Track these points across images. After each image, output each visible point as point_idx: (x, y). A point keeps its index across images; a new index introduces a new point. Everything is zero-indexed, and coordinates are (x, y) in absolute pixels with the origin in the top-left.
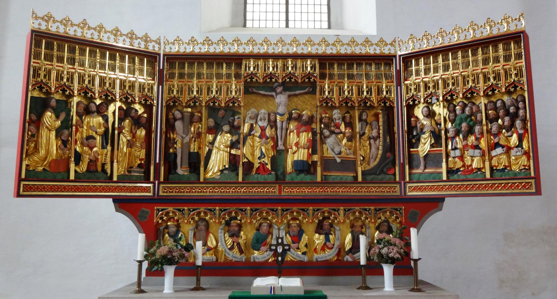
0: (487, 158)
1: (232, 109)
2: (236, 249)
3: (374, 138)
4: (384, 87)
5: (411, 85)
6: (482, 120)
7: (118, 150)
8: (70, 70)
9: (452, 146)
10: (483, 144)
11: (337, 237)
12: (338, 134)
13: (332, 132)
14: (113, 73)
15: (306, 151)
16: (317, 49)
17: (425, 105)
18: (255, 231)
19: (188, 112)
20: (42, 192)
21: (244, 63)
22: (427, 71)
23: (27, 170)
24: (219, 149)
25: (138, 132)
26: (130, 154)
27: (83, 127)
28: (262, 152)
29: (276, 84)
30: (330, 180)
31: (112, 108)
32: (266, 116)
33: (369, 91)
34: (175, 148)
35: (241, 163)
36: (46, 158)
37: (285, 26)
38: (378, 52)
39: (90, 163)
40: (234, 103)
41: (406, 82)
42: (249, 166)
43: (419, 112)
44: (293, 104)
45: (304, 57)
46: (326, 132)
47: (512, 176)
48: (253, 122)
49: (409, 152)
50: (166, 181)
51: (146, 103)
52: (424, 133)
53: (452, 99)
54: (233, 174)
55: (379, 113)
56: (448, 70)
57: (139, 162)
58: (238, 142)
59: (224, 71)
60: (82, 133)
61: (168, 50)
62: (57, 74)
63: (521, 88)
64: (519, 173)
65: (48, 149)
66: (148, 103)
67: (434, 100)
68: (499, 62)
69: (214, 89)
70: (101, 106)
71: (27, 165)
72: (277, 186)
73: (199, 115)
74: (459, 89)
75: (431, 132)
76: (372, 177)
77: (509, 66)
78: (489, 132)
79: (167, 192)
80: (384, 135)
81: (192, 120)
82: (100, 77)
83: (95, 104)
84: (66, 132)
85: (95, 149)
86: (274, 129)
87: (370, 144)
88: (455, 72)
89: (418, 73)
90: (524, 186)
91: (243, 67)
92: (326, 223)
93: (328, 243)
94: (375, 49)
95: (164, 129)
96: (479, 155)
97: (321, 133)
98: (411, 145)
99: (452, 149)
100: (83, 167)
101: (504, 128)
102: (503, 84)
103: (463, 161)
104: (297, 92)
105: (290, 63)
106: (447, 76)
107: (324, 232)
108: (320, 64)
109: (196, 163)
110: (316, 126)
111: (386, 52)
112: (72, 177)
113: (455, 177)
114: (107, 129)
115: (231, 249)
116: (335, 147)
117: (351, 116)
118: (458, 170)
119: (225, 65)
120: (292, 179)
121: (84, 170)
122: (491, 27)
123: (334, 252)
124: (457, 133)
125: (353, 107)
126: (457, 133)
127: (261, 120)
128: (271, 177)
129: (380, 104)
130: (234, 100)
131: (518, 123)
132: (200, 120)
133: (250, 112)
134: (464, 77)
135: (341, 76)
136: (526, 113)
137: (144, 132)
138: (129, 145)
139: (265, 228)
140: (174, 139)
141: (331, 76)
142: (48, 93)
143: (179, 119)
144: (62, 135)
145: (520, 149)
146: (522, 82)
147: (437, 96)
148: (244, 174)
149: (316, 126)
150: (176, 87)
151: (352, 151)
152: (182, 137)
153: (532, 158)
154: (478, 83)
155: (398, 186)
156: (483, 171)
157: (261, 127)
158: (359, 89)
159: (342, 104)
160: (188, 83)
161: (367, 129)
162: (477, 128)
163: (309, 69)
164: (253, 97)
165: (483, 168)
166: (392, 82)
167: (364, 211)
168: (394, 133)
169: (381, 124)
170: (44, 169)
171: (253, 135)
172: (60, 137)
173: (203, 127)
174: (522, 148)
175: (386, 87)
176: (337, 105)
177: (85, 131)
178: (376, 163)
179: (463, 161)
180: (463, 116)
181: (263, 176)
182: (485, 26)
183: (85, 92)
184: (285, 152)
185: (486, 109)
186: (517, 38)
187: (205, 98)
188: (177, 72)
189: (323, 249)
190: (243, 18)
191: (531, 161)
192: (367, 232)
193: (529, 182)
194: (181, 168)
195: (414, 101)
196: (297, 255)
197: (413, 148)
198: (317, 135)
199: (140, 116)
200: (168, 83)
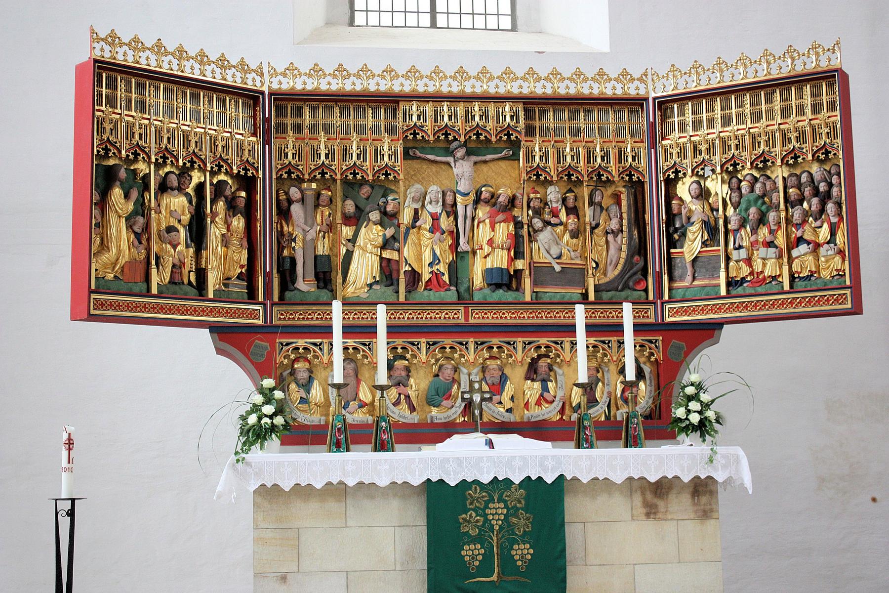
0: (785, 260)
1: (383, 184)
2: (404, 406)
4: (629, 150)
5: (671, 146)
11: (559, 385)
12: (557, 225)
13: (547, 223)
15: (505, 252)
16: (521, 87)
17: (695, 178)
18: (431, 379)
22: (697, 125)
24: (364, 250)
28: (434, 254)
29: (456, 144)
30: (546, 300)
32: (440, 195)
33: (605, 156)
39: (174, 270)
40: (387, 175)
41: (663, 142)
42: (414, 277)
43: (684, 189)
46: (538, 223)
47: (820, 286)
49: (669, 253)
53: (736, 171)
54: (389, 290)
56: (729, 125)
58: (393, 237)
59: (370, 121)
61: (275, 86)
64: (831, 281)
67: (708, 172)
69: (355, 151)
71: (96, 270)
72: (462, 308)
73: (330, 193)
74: (745, 154)
75: (704, 222)
76: (610, 294)
78: (788, 221)
80: (629, 228)
82: (183, 131)
84: (141, 220)
85: (179, 248)
87: (607, 242)
88: (740, 127)
89: (682, 127)
90: (837, 300)
91: (400, 115)
92: (543, 363)
94: (614, 88)
97: (530, 225)
98: (672, 244)
99: (735, 249)
101: (811, 215)
103: (751, 266)
104: (489, 157)
105: (477, 108)
106: (728, 134)
108: (526, 110)
111: (633, 92)
112: (154, 290)
113: (740, 290)
115: (396, 403)
116: (550, 246)
117: (576, 197)
120: (485, 297)
121: (167, 280)
122: (793, 59)
123: (557, 405)
124: (743, 224)
125: (579, 182)
126: (743, 224)
127: (431, 203)
128: (451, 295)
130: (386, 171)
131: (830, 207)
133: (413, 189)
134: (753, 137)
135: (559, 131)
136: (841, 192)
139: (448, 372)
140: (290, 234)
143: (297, 201)
144: (134, 224)
147: (712, 165)
148: (408, 291)
149: (523, 214)
151: (578, 254)
152: (304, 230)
153: (847, 258)
155: (652, 308)
156: (780, 279)
157: (432, 215)
158: (588, 153)
160: (311, 141)
161: (602, 219)
162: (772, 216)
163: (508, 119)
164: (415, 164)
165: (779, 276)
166: (642, 142)
167: (602, 345)
169: (624, 209)
170: (115, 277)
171: (420, 228)
172: (131, 227)
174: (835, 245)
175: (633, 149)
176: (555, 178)
178: (617, 272)
179: (751, 266)
181: (437, 294)
182: (784, 57)
184: (471, 255)
186: (833, 78)
188: (289, 121)
189: (538, 403)
191: (847, 262)
192: (606, 377)
193: (845, 296)
195: (677, 172)
197: (675, 248)
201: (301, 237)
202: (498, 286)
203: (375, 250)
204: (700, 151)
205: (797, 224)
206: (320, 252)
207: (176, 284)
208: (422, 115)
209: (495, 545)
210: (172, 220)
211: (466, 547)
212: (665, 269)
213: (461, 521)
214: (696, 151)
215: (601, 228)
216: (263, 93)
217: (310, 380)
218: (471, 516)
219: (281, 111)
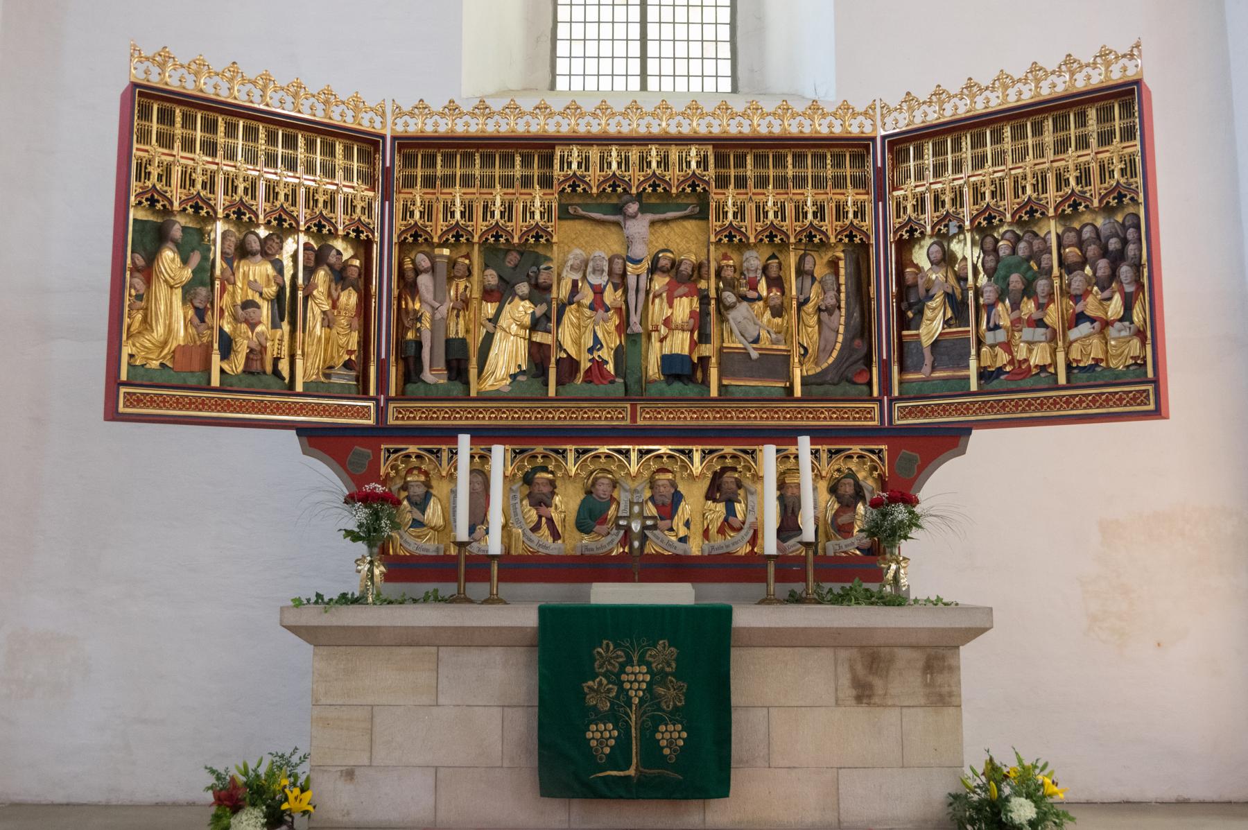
2: (545, 530)
3: (827, 309)
5: (905, 198)
6: (1051, 267)
7: (304, 331)
8: (208, 166)
9: (988, 322)
10: (1053, 316)
12: (753, 300)
13: (744, 298)
14: (291, 174)
19: (442, 256)
20: (161, 408)
21: (558, 153)
22: (939, 170)
25: (343, 298)
26: (327, 340)
27: (234, 284)
30: (737, 396)
31: (290, 246)
34: (418, 330)
35: (553, 360)
36: (165, 343)
37: (638, 88)
42: (569, 367)
43: (921, 256)
44: (661, 240)
45: (683, 141)
48: (577, 276)
49: (900, 337)
50: (402, 396)
51: (358, 236)
52: (931, 298)
54: (537, 383)
55: (839, 259)
57: (347, 357)
58: (547, 316)
60: (233, 294)
61: (400, 129)
62: (184, 173)
63: (1132, 199)
64: (1124, 373)
65: (170, 324)
66: (363, 236)
68: (1087, 146)
70: (270, 243)
71: (131, 356)
73: (467, 261)
75: (947, 294)
77: (1107, 155)
79: (403, 418)
81: (453, 271)
82: (268, 181)
83: (257, 235)
84: (203, 291)
85: (259, 329)
86: (620, 292)
89: (920, 175)
91: (557, 162)
93: (731, 519)
95: (395, 292)
96: (1043, 338)
97: (719, 300)
99: (989, 329)
100: (238, 363)
102: (1095, 189)
103: (1011, 353)
105: (654, 153)
106: (980, 178)
107: (724, 497)
110: (710, 285)
111: (855, 131)
112: (215, 381)
113: (995, 384)
114: (281, 289)
115: (536, 528)
116: (750, 325)
117: (780, 264)
118: (1000, 371)
119: (518, 159)
121: (240, 369)
123: (746, 534)
125: (784, 245)
128: (618, 389)
129: (841, 240)
130: (539, 234)
131: (1125, 271)
132: (469, 273)
136: (1141, 250)
137: (354, 299)
138: (326, 323)
141: (741, 182)
142: (167, 212)
143: (426, 271)
145: (1127, 323)
146: (1133, 187)
148: (559, 383)
149: (710, 285)
150: (418, 203)
153: (1149, 341)
154: (1045, 191)
155: (876, 406)
159: (761, 240)
162: (1041, 284)
164: (578, 225)
165: (1050, 365)
168: (870, 300)
169: (842, 280)
170: (162, 365)
171: (579, 304)
172: (191, 301)
173: (475, 287)
174: (1132, 322)
177: (241, 292)
179: (1011, 353)
180: (1014, 259)
183: (240, 215)
185: (1060, 246)
186: (1126, 96)
187: (479, 225)
188: (419, 172)
189: (721, 531)
190: (548, 68)
191: (1149, 348)
194: (431, 370)
195: (911, 231)
196: (670, 544)
198: (709, 304)
199: (346, 266)
200: (402, 196)
201: (428, 315)
202: (678, 377)
203: (522, 332)
204: (943, 203)
205: (1076, 296)
206: (452, 335)
207: (252, 373)
208: (585, 163)
209: (633, 725)
210: (250, 292)
211: (593, 727)
212: (895, 357)
213: (586, 690)
214: (938, 202)
215: (811, 304)
216: (383, 137)
217: (427, 496)
218: (600, 683)
219: (409, 161)
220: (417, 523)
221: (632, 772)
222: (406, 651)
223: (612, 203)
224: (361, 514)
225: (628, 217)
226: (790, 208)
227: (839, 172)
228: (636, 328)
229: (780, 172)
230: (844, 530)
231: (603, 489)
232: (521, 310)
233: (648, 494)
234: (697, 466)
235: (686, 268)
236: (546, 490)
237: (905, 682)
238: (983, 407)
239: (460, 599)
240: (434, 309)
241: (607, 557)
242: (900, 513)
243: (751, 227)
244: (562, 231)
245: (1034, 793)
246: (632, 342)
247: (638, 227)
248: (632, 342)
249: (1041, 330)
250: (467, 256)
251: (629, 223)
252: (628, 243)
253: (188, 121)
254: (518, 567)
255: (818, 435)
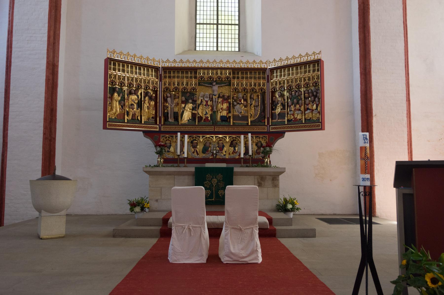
2: (195, 153)
13: (238, 103)
21: (198, 71)
23: (109, 118)
25: (151, 103)
36: (115, 113)
38: (259, 67)
42: (200, 118)
48: (202, 98)
49: (272, 112)
50: (164, 124)
52: (278, 104)
59: (189, 75)
60: (129, 103)
61: (163, 65)
75: (281, 103)
81: (175, 97)
85: (134, 110)
95: (163, 102)
97: (233, 104)
100: (130, 117)
103: (294, 116)
109: (177, 117)
110: (231, 100)
111: (263, 67)
112: (126, 121)
113: (290, 123)
114: (139, 101)
115: (194, 153)
116: (240, 109)
118: (292, 120)
119: (189, 73)
123: (238, 154)
125: (247, 92)
130: (194, 89)
131: (317, 99)
132: (178, 97)
137: (154, 103)
141: (238, 78)
148: (198, 122)
149: (231, 100)
162: (300, 101)
164: (202, 87)
175: (263, 83)
179: (294, 116)
187: (181, 87)
188: (167, 75)
189: (233, 153)
195: (274, 89)
199: (152, 96)
212: (270, 116)
216: (160, 67)
217: (170, 146)
219: (165, 72)
220: (168, 152)
221: (213, 199)
222: (168, 176)
223: (210, 82)
224: (159, 149)
225: (213, 85)
226: (248, 84)
227: (260, 76)
228: (215, 110)
229: (247, 76)
230: (258, 153)
231: (208, 144)
232: (190, 106)
233: (217, 145)
234: (228, 140)
235: (226, 97)
236: (196, 144)
237: (268, 182)
238: (288, 127)
239: (178, 166)
240: (171, 105)
241: (209, 158)
242: (268, 149)
243: (240, 88)
244: (198, 88)
245: (293, 204)
246: (214, 113)
247: (216, 88)
248: (214, 113)
249: (300, 111)
250: (178, 94)
251: (214, 87)
252: (213, 91)
253: (119, 65)
254: (190, 161)
255: (252, 133)
